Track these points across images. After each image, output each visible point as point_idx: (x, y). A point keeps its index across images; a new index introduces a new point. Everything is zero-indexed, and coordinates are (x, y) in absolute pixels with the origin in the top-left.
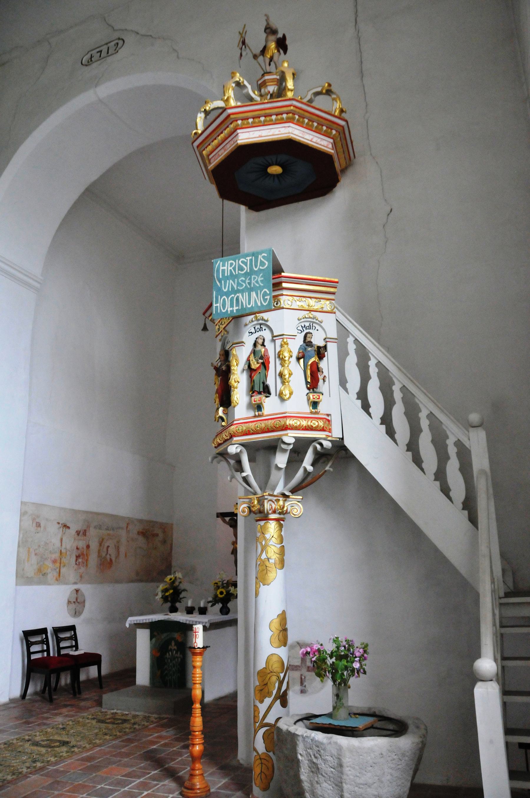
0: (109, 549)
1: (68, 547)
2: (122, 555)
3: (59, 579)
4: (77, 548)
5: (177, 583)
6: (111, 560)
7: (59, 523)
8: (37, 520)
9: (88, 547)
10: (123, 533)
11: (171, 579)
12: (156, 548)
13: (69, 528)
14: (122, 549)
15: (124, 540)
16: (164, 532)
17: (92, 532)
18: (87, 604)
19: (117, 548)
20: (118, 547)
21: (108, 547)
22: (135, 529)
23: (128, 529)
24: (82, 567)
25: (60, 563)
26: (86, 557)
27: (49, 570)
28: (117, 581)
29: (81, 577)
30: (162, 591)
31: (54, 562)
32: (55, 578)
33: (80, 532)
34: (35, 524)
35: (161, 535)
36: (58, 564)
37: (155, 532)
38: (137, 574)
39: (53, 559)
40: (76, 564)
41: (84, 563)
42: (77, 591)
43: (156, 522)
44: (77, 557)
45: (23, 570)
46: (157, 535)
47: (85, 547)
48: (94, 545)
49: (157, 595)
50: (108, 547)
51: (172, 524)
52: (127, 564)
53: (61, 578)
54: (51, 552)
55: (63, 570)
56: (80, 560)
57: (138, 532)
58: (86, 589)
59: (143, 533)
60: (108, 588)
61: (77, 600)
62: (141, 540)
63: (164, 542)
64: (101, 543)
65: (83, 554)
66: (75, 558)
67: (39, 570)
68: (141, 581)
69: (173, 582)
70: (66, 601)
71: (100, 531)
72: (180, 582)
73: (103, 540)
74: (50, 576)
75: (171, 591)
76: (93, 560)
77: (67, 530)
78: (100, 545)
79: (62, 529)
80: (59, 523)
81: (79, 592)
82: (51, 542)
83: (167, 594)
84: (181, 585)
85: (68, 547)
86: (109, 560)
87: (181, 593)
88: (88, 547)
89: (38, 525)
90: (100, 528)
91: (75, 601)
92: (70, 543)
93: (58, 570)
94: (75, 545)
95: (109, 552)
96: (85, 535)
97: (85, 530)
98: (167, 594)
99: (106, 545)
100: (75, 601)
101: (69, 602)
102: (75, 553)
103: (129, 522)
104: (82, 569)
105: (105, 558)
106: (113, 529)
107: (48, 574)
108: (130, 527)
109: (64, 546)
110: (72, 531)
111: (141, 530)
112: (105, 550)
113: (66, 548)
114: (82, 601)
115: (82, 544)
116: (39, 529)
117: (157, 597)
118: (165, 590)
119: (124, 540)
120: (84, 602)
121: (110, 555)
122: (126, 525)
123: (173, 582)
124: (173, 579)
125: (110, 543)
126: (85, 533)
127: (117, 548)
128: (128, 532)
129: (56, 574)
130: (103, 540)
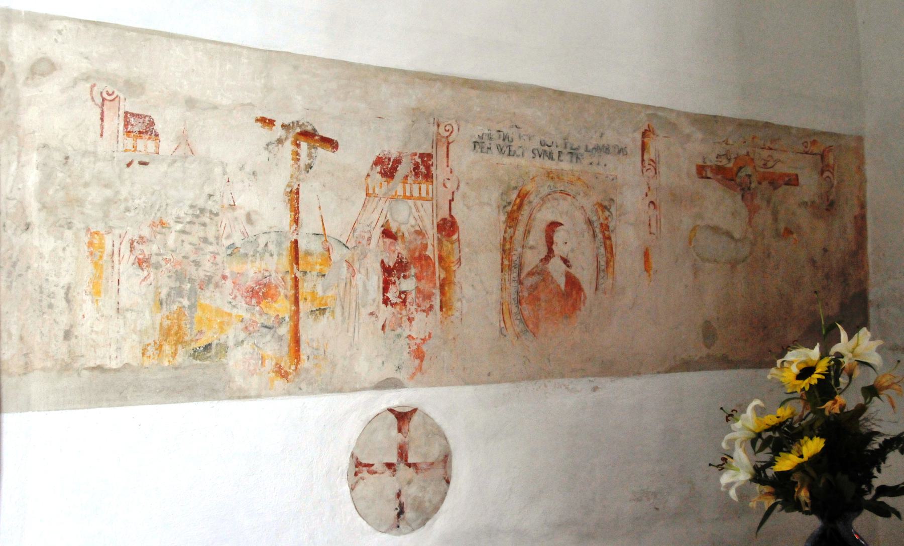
0: (559, 236)
1: (336, 228)
2: (627, 260)
3: (293, 366)
4: (387, 233)
5: (848, 398)
6: (573, 283)
7: (267, 122)
8: (131, 105)
9: (448, 227)
10: (626, 170)
11: (806, 372)
12: (788, 232)
13: (330, 143)
14: (628, 238)
15: (632, 200)
16: (824, 168)
17: (463, 161)
18: (462, 470)
19: (603, 234)
20: (605, 227)
21: (553, 226)
22: (679, 158)
23: (651, 154)
24: (419, 317)
25: (296, 302)
26: (440, 273)
27: (232, 334)
28: (610, 368)
29: (419, 355)
30: (757, 441)
31: (260, 293)
32: (270, 365)
33: (398, 162)
34: (115, 123)
35: (810, 183)
36: (282, 306)
37: (780, 169)
38: (708, 333)
39: (250, 282)
40: (386, 301)
41: (428, 297)
42: (402, 417)
43: (787, 129)
44: (391, 273)
45: (67, 335)
46: (793, 181)
47: (432, 231)
48: (479, 220)
49: (724, 463)
50: (553, 226)
51: (860, 139)
52: (651, 297)
53: (305, 364)
54: (233, 251)
55: (310, 330)
56: (408, 285)
57: (701, 170)
58: (450, 407)
59: (725, 174)
60: (567, 401)
61: (402, 453)
62: (719, 206)
63: (827, 206)
64: (515, 211)
65: (422, 259)
66: (376, 279)
67: (172, 334)
68: (726, 362)
69: (826, 389)
70: (345, 462)
71: (507, 160)
72: (871, 392)
73: (523, 196)
74: (237, 359)
75: (813, 446)
76: (479, 278)
77: (322, 153)
78: (512, 219)
79: (289, 146)
80: (267, 122)
81: (416, 419)
82: (233, 206)
83: (786, 463)
84: (877, 406)
85: (336, 228)
86: (562, 281)
87: (879, 457)
88: (448, 227)
89: (142, 127)
90: (506, 147)
91: (394, 459)
92: (342, 206)
93: (284, 330)
94: (374, 219)
95: (559, 249)
96: (428, 176)
97: (426, 158)
98: (786, 463)
99: (546, 215)
100: (394, 459)
101: (360, 467)
102: (378, 253)
103: (652, 125)
104: (422, 324)
105: (541, 272)
106: (574, 154)
107: (224, 348)
108: (656, 145)
109: (310, 222)
110: (356, 156)
111: (712, 160)
112: (537, 237)
113: (321, 235)
114: (435, 453)
115: (413, 215)
116: (146, 145)
117: (725, 478)
118: (780, 438)
119: (632, 200)
120: (446, 459)
121: (565, 261)
122: (638, 136)
123: (826, 389)
124: (822, 367)
125: (570, 214)
126: (423, 168)
127: (603, 234)
128: (649, 165)
129: (274, 349)
130: (523, 196)
